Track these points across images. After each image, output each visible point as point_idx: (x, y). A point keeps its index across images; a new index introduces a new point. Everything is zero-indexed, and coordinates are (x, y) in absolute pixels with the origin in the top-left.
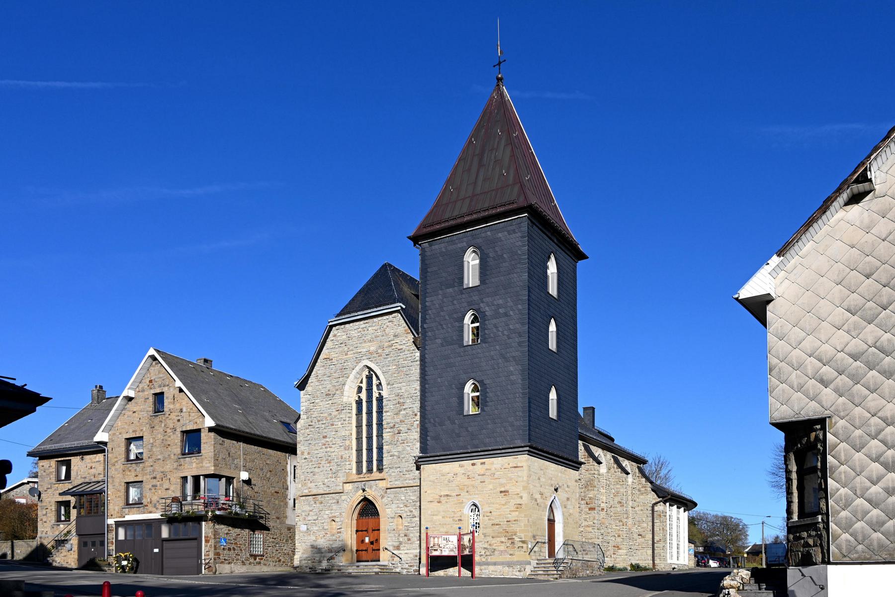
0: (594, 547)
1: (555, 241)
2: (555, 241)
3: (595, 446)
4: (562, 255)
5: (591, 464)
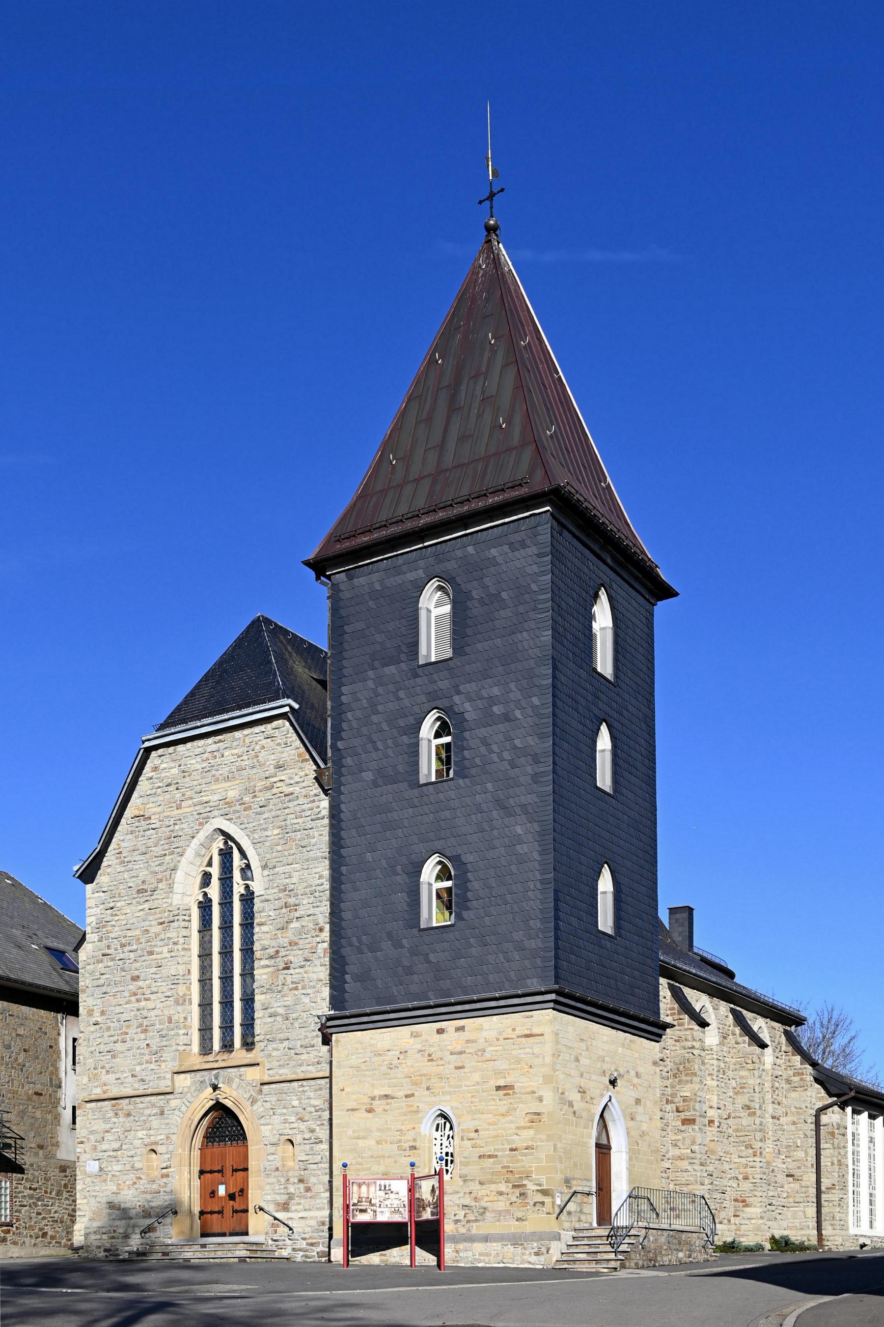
0: (693, 1202)
1: (609, 561)
2: (609, 561)
3: (694, 989)
4: (623, 590)
5: (686, 1026)
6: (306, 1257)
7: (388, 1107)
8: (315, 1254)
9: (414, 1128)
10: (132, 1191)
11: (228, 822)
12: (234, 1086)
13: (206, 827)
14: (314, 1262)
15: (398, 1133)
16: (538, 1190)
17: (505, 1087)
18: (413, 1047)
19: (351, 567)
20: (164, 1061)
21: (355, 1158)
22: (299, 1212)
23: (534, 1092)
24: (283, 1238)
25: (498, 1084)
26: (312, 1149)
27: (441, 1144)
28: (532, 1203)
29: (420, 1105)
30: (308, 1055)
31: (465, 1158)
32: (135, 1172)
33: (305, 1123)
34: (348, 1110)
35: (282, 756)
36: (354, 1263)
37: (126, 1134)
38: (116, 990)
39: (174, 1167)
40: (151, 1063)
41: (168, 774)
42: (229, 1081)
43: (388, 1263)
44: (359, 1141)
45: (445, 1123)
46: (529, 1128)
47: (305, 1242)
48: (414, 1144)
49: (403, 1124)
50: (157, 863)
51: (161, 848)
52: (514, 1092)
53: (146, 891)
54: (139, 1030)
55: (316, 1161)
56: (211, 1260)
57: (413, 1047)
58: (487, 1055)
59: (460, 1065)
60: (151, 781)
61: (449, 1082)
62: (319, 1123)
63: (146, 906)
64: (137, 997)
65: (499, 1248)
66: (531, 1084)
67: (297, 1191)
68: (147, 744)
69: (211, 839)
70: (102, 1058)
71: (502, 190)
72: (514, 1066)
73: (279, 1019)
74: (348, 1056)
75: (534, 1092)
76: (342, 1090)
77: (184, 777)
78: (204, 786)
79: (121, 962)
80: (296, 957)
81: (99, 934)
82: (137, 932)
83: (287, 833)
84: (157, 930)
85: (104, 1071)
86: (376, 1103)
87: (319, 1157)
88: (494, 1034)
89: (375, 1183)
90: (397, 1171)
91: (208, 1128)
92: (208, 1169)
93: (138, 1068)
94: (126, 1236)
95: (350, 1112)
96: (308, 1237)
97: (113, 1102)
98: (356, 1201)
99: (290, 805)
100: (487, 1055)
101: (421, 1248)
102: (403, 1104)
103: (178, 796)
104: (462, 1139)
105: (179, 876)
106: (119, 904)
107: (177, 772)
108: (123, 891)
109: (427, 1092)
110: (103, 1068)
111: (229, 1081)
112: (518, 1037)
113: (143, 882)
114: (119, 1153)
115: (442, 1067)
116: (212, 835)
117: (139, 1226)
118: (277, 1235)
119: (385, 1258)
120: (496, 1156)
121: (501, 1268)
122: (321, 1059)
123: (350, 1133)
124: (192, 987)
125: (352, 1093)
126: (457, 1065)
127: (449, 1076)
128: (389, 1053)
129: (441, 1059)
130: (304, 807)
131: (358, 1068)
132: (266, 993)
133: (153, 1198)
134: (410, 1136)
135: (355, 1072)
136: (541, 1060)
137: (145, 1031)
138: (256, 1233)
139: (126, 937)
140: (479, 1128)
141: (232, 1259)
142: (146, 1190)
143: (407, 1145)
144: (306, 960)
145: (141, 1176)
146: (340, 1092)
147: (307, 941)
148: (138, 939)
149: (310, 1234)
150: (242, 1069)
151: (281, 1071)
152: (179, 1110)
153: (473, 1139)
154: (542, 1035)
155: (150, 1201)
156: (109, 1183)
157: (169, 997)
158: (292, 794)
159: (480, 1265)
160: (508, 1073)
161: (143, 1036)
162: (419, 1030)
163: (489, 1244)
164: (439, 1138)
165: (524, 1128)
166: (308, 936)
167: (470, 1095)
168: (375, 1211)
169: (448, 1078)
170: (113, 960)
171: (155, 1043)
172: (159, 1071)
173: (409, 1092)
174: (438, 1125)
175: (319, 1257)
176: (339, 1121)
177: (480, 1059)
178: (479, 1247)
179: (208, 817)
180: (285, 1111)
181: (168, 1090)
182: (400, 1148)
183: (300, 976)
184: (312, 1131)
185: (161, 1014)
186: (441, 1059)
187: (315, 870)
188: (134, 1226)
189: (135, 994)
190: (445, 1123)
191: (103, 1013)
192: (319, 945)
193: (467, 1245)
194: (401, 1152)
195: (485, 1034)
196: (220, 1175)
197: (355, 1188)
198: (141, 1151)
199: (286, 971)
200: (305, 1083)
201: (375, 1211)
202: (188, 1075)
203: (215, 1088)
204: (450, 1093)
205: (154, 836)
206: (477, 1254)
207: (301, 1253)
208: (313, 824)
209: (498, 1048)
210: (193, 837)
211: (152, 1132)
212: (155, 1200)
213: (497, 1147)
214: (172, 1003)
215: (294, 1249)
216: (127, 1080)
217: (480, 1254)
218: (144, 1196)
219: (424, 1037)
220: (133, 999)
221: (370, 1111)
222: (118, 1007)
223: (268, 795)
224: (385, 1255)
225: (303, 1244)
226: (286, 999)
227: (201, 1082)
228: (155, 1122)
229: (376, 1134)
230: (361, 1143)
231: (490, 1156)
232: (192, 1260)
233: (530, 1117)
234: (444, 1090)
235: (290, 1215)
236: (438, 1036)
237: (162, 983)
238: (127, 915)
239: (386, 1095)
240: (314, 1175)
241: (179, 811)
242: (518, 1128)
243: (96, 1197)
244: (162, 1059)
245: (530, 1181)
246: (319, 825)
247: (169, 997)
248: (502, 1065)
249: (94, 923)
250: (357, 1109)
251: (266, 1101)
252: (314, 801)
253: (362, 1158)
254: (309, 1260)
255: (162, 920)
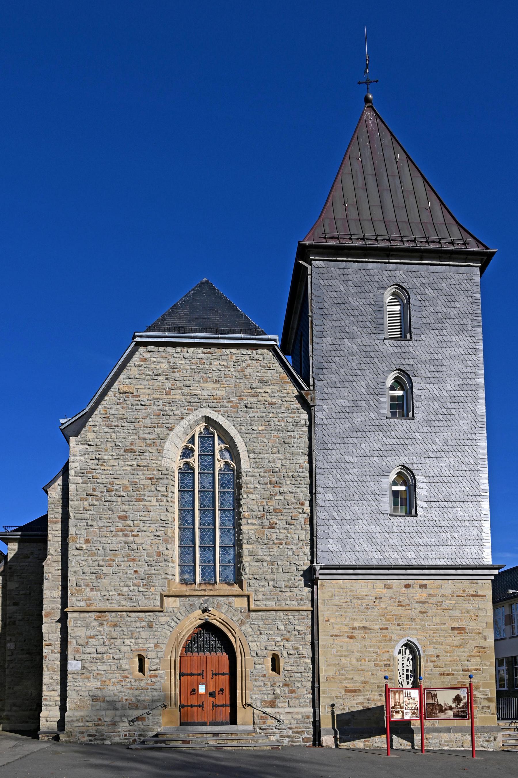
6: (293, 742)
7: (366, 635)
8: (301, 739)
9: (388, 652)
10: (119, 687)
11: (217, 414)
12: (224, 610)
13: (195, 413)
14: (300, 746)
15: (375, 654)
16: (485, 698)
17: (459, 628)
18: (386, 595)
19: (330, 259)
20: (153, 586)
21: (339, 671)
22: (284, 708)
23: (480, 633)
24: (271, 727)
25: (453, 626)
26: (296, 662)
27: (403, 664)
28: (480, 707)
29: (392, 635)
30: (291, 593)
31: (429, 674)
32: (121, 672)
33: (289, 643)
34: (332, 636)
35: (266, 375)
36: (342, 747)
37: (112, 640)
38: (103, 524)
39: (162, 670)
40: (140, 586)
41: (157, 367)
42: (219, 607)
43: (371, 747)
44: (342, 658)
45: (405, 650)
46: (477, 656)
47: (291, 731)
48: (388, 663)
49: (379, 648)
50: (146, 432)
51: (150, 421)
52: (465, 632)
53: (135, 452)
54: (126, 559)
55: (300, 671)
56: (244, 748)
57: (386, 595)
58: (444, 606)
59: (424, 610)
60: (141, 368)
61: (415, 622)
62: (302, 643)
63: (134, 463)
64: (124, 532)
65: (460, 737)
66: (478, 627)
67: (283, 692)
68: (138, 339)
69: (197, 423)
70: (87, 578)
71: (377, 81)
72: (465, 615)
73: (265, 564)
74: (332, 596)
75: (480, 633)
76: (328, 621)
77: (173, 372)
78: (193, 382)
79: (107, 503)
80: (281, 522)
81: (84, 477)
82: (126, 482)
83: (271, 431)
84: (147, 483)
85: (88, 588)
86: (356, 632)
87: (303, 668)
88: (449, 592)
89: (403, 691)
90: (375, 681)
91: (187, 640)
92: (189, 672)
93: (125, 589)
94: (114, 724)
95: (333, 637)
96: (294, 727)
97: (98, 614)
98: (393, 705)
99: (274, 411)
100: (444, 606)
101: (397, 736)
102: (379, 635)
103: (167, 384)
104: (427, 661)
105: (168, 445)
106: (106, 457)
107: (167, 367)
108: (111, 448)
109: (398, 628)
110: (87, 585)
111: (219, 607)
112: (467, 596)
113: (132, 444)
114: (105, 655)
115: (410, 611)
116: (199, 420)
117: (127, 717)
118: (266, 725)
119: (368, 743)
120: (453, 674)
121: (461, 750)
122: (304, 597)
123: (334, 651)
124: (175, 531)
125: (335, 624)
126: (421, 610)
127: (415, 618)
128: (366, 597)
129: (409, 605)
130: (286, 415)
131: (340, 607)
132: (253, 544)
133: (141, 693)
134: (386, 656)
135: (338, 609)
136: (485, 612)
137: (133, 560)
138: (245, 723)
139: (113, 484)
140: (439, 654)
141: (265, 748)
142: (133, 687)
143: (382, 663)
144: (289, 524)
145: (128, 675)
146: (325, 622)
147: (290, 511)
148: (127, 488)
149: (296, 725)
150: (231, 599)
151: (268, 603)
152: (169, 625)
153: (435, 662)
154: (485, 596)
155: (138, 696)
156: (92, 680)
157: (158, 536)
158: (275, 404)
159: (446, 748)
160: (461, 619)
161: (132, 564)
162: (391, 584)
163: (452, 734)
164: (401, 659)
165: (474, 656)
166: (292, 507)
167: (432, 632)
168: (403, 712)
169: (414, 619)
170: (99, 500)
171: (143, 570)
172: (147, 593)
173: (383, 626)
174: (400, 650)
175: (304, 742)
176: (324, 643)
177: (439, 608)
178: (444, 736)
179: (197, 406)
180: (271, 632)
181: (158, 608)
182: (376, 665)
183: (284, 535)
184: (296, 649)
185: (150, 548)
186: (409, 605)
187: (298, 462)
188: (121, 717)
189: (122, 530)
190: (405, 650)
191: (87, 541)
192: (301, 515)
193: (435, 734)
194: (378, 668)
195: (443, 591)
196: (199, 677)
197: (393, 695)
198: (129, 656)
199: (271, 530)
200: (289, 613)
201: (403, 712)
202: (178, 599)
203: (205, 610)
204: (416, 629)
205: (143, 411)
206: (443, 741)
207: (288, 739)
208: (293, 428)
209: (452, 602)
210: (182, 418)
211: (140, 641)
212: (143, 695)
213: (453, 668)
214: (161, 541)
215: (281, 736)
216: (113, 597)
217: (445, 741)
218: (132, 692)
219: (395, 589)
220: (121, 533)
221: (351, 637)
222: (104, 538)
223: (254, 400)
224: (368, 741)
225: (290, 733)
226: (271, 550)
227: (191, 605)
228: (144, 634)
229: (357, 654)
230: (343, 660)
231: (448, 674)
232: (224, 748)
233: (477, 649)
234: (411, 627)
235: (277, 710)
236: (406, 589)
237: (151, 525)
238: (114, 467)
239: (364, 627)
240: (298, 682)
241: (168, 397)
242: (468, 656)
243: (77, 691)
244: (151, 584)
245: (478, 692)
246: (299, 430)
247: (158, 536)
248: (456, 613)
249: (78, 468)
250: (341, 636)
251: (254, 624)
252: (294, 413)
253: (345, 670)
254: (295, 744)
255: (151, 476)
